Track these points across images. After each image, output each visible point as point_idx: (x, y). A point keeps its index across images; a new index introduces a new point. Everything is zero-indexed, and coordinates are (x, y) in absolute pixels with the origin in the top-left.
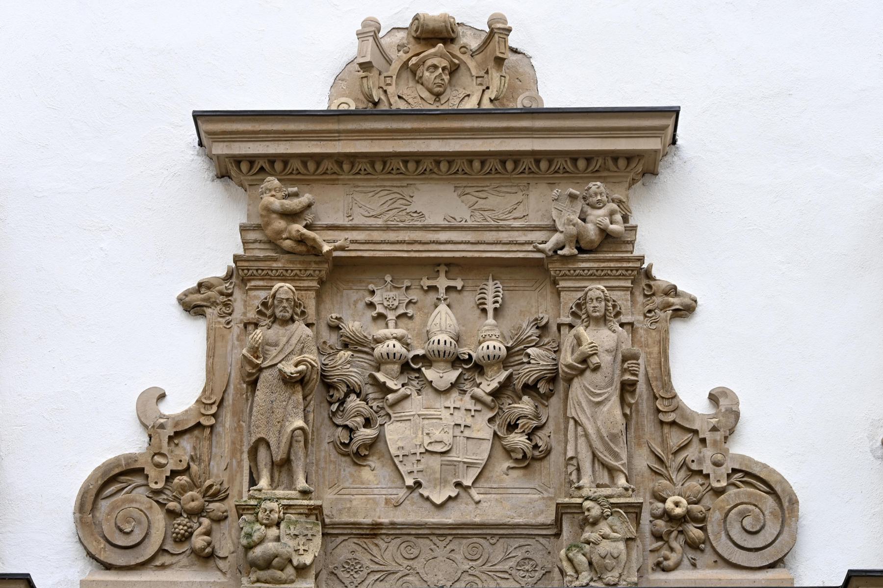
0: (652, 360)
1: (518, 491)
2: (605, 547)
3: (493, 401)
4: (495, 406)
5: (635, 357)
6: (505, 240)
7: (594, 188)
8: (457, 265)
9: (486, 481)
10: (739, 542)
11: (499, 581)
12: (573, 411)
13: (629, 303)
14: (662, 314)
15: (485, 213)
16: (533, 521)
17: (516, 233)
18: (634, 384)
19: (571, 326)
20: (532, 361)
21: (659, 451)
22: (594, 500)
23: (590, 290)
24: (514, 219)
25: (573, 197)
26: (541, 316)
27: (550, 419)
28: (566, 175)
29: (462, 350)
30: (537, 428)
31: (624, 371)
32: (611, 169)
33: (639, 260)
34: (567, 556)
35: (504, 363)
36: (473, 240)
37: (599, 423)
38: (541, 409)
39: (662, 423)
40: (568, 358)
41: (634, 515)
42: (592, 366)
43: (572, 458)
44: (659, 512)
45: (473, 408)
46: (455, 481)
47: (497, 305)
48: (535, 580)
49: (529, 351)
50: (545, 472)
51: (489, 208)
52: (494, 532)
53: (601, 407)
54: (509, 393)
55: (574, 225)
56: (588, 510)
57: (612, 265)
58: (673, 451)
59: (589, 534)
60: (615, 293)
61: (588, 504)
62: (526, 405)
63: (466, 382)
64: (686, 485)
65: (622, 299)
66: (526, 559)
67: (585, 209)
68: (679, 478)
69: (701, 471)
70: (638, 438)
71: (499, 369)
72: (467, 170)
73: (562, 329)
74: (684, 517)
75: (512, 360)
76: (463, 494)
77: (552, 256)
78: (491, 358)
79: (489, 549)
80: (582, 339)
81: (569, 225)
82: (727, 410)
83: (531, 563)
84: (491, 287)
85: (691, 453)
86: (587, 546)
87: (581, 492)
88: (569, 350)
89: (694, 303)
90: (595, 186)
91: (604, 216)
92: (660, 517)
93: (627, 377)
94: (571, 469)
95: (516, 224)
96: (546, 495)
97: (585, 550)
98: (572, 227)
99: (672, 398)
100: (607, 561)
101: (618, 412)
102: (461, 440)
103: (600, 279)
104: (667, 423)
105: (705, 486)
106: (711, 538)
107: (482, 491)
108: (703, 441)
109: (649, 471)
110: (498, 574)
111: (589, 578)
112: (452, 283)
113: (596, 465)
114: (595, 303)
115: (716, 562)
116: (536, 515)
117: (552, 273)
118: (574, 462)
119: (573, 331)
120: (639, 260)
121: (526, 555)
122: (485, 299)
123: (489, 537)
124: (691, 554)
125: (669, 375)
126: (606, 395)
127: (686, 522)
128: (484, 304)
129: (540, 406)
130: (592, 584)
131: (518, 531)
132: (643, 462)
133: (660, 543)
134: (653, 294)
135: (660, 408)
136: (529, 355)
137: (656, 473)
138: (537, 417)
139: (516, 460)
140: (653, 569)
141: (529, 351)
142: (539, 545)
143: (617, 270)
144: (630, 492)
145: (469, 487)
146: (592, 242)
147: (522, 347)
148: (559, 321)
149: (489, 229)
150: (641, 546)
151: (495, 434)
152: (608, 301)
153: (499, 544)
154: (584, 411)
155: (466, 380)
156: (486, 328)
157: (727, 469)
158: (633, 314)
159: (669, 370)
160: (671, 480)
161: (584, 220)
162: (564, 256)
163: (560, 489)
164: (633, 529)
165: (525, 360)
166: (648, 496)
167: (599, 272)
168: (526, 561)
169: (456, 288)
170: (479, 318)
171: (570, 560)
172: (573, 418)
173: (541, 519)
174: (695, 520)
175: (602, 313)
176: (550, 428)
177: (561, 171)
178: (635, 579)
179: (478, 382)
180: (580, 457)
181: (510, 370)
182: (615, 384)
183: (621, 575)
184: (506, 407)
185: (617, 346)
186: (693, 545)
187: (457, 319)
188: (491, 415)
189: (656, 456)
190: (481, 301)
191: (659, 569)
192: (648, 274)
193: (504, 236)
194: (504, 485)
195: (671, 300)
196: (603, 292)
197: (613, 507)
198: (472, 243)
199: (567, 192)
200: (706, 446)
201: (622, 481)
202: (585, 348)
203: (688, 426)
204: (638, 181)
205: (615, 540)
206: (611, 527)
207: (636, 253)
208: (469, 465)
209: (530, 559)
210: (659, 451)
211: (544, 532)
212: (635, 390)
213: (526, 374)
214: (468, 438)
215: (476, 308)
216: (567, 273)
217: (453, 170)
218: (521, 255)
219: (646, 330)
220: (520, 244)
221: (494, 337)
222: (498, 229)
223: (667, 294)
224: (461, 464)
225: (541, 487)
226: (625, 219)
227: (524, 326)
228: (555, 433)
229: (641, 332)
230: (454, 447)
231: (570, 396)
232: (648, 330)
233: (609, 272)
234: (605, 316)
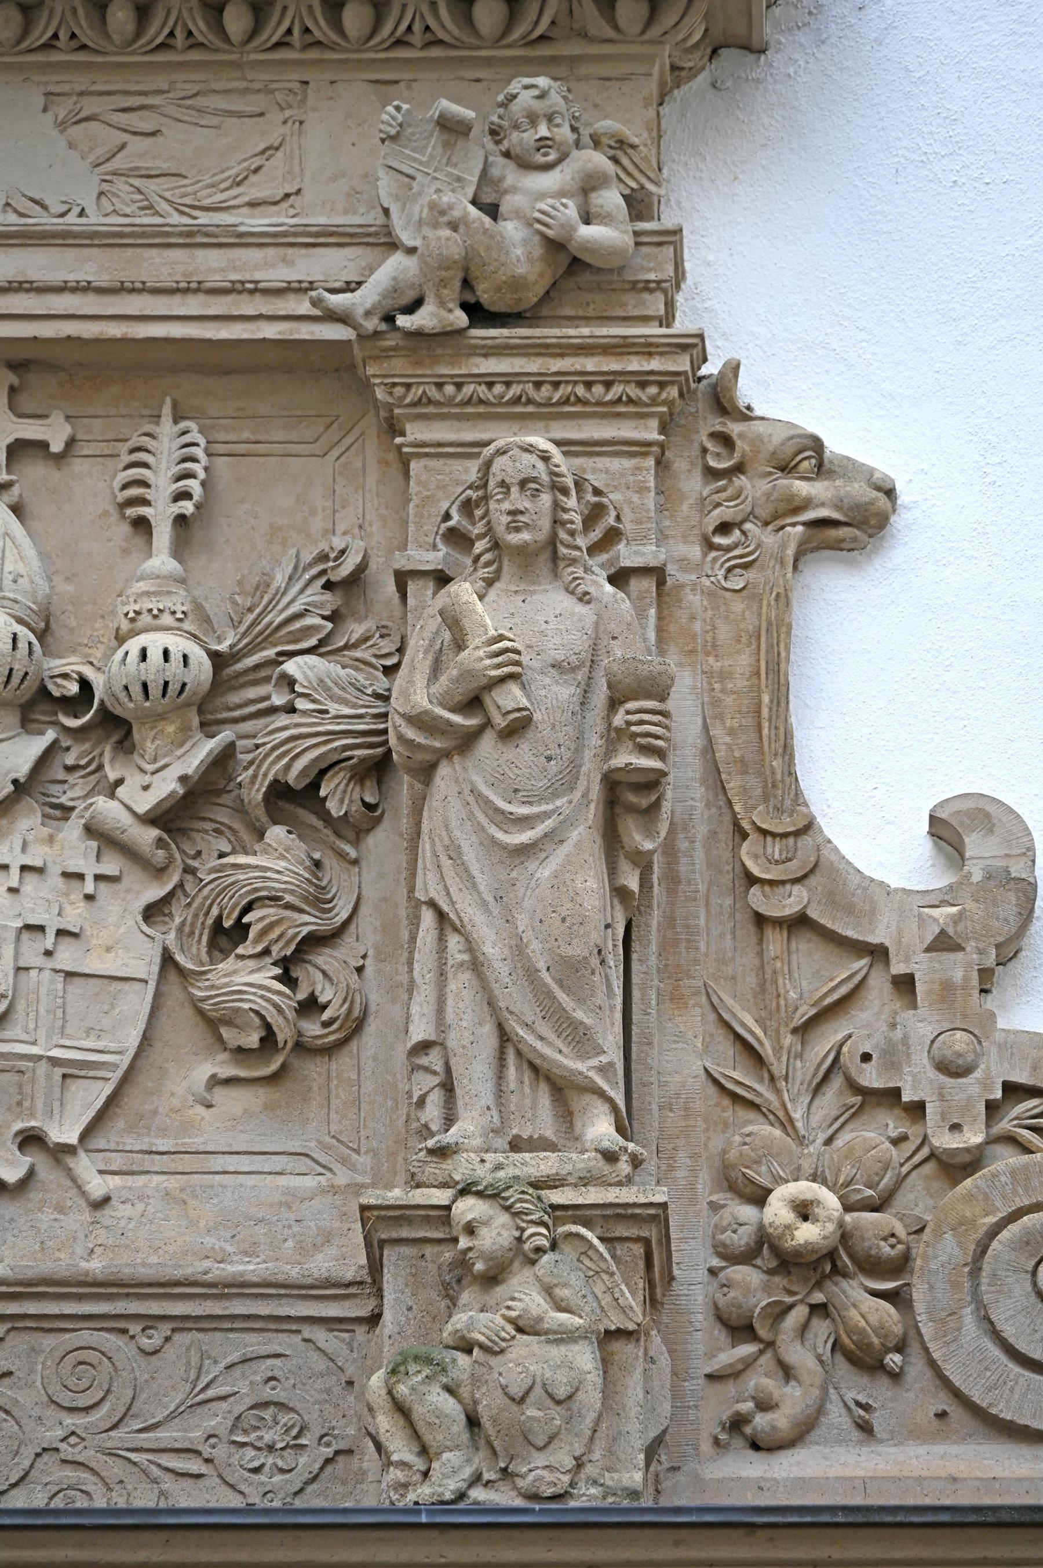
0: (729, 700)
1: (244, 1163)
2: (527, 1361)
3: (160, 843)
4: (171, 859)
5: (658, 689)
6: (215, 279)
7: (526, 98)
8: (52, 367)
9: (131, 1128)
10: (1022, 1346)
11: (168, 1483)
12: (432, 877)
13: (651, 500)
14: (769, 539)
15: (151, 186)
16: (293, 1273)
17: (255, 255)
18: (651, 783)
19: (442, 579)
20: (301, 704)
21: (750, 1022)
22: (492, 1194)
23: (501, 452)
24: (252, 204)
25: (452, 129)
26: (338, 543)
27: (364, 910)
28: (435, 52)
29: (57, 664)
30: (314, 941)
31: (615, 737)
32: (593, 32)
33: (684, 347)
34: (390, 1393)
35: (207, 708)
36: (102, 280)
37: (522, 922)
38: (333, 871)
39: (760, 920)
40: (417, 692)
41: (638, 1249)
42: (500, 721)
43: (424, 1046)
44: (742, 1238)
45: (90, 868)
46: (19, 1126)
47: (187, 507)
48: (295, 1482)
49: (290, 667)
50: (341, 1096)
51: (164, 166)
52: (155, 1308)
53: (532, 865)
54: (223, 816)
55: (454, 226)
56: (470, 1230)
57: (590, 364)
58: (798, 1021)
59: (473, 1317)
60: (602, 462)
61: (468, 1209)
62: (277, 859)
63: (72, 778)
64: (839, 1142)
65: (624, 483)
66: (266, 1404)
67: (495, 172)
68: (815, 1119)
69: (896, 1092)
70: (673, 974)
71: (185, 730)
72: (87, 35)
73: (412, 587)
74: (832, 1255)
75: (234, 698)
76: (47, 1173)
77: (376, 334)
78: (155, 691)
79: (142, 1369)
80: (466, 623)
81: (435, 226)
82: (989, 877)
83: (285, 1418)
84: (166, 441)
85: (864, 1027)
86: (463, 1359)
87: (448, 1165)
88: (424, 665)
89: (883, 501)
90: (531, 89)
91: (562, 193)
92: (746, 1257)
93: (626, 758)
94: (426, 1082)
95: (257, 222)
96: (342, 1177)
97: (454, 1373)
98: (446, 232)
99: (797, 834)
100: (532, 1412)
101: (590, 885)
102: (43, 983)
103: (547, 413)
104: (778, 923)
105: (909, 1147)
106: (927, 1330)
107: (117, 1162)
108: (905, 984)
109: (712, 1090)
110: (166, 1460)
111: (467, 1472)
112: (31, 430)
113: (512, 1072)
114: (518, 500)
115: (942, 1415)
116: (304, 1250)
117: (380, 394)
118: (433, 1059)
119: (443, 598)
120: (684, 347)
121: (268, 1393)
122: (144, 484)
123: (135, 1328)
124: (855, 1387)
125: (787, 751)
126: (549, 824)
127: (838, 1271)
128: (145, 502)
129: (331, 863)
130: (478, 1494)
131: (239, 1307)
132: (684, 1057)
133: (747, 1349)
134: (739, 469)
135: (756, 871)
136: (290, 682)
137: (735, 1098)
138: (319, 900)
139: (241, 1053)
140: (717, 1442)
141: (290, 667)
142: (315, 1356)
143: (608, 385)
144: (624, 1167)
145: (69, 1150)
146: (517, 284)
147: (270, 653)
148: (401, 563)
149: (161, 239)
150: (664, 1361)
151: (167, 959)
152: (565, 491)
153: (170, 1353)
154: (471, 878)
155: (70, 769)
156: (142, 586)
157: (986, 1084)
158: (662, 537)
159: (788, 735)
160: (787, 1124)
161: (493, 211)
162: (417, 334)
163: (392, 1155)
164: (632, 1299)
165: (278, 700)
166: (704, 1180)
167: (546, 390)
168: (268, 1414)
169: (44, 445)
170: (125, 551)
171: (402, 1410)
172: (432, 904)
173: (322, 1265)
174: (872, 1266)
175: (543, 535)
176: (366, 936)
177: (417, 37)
178: (636, 1478)
179: (112, 776)
180: (451, 1044)
181: (226, 735)
182: (582, 783)
183: (579, 1464)
184: (205, 867)
185: (594, 649)
186: (865, 1359)
187: (44, 557)
188: (155, 892)
189: (738, 1037)
190: (134, 492)
191: (738, 1443)
192: (722, 399)
193: (213, 265)
194: (196, 1142)
195: (802, 488)
196: (546, 458)
197: (558, 1221)
198: (101, 291)
199: (434, 113)
200: (915, 1006)
201: (601, 1128)
202: (475, 656)
203: (850, 933)
204: (694, 73)
205: (564, 1337)
206: (548, 1291)
207: (683, 324)
208: (71, 1072)
209: (280, 1405)
210: (747, 1021)
211: (332, 1310)
212: (656, 806)
213: (279, 748)
214: (69, 975)
215: (114, 516)
216: (433, 393)
217: (40, 34)
218: (270, 331)
219: (710, 594)
220: (266, 292)
221: (167, 619)
222: (192, 239)
223: (786, 468)
224: (43, 1067)
225: (324, 1147)
226: (639, 205)
227: (280, 579)
228: (380, 959)
229: (695, 600)
230: (21, 1006)
231: (425, 826)
232: (713, 595)
233: (580, 391)
234: (553, 542)
